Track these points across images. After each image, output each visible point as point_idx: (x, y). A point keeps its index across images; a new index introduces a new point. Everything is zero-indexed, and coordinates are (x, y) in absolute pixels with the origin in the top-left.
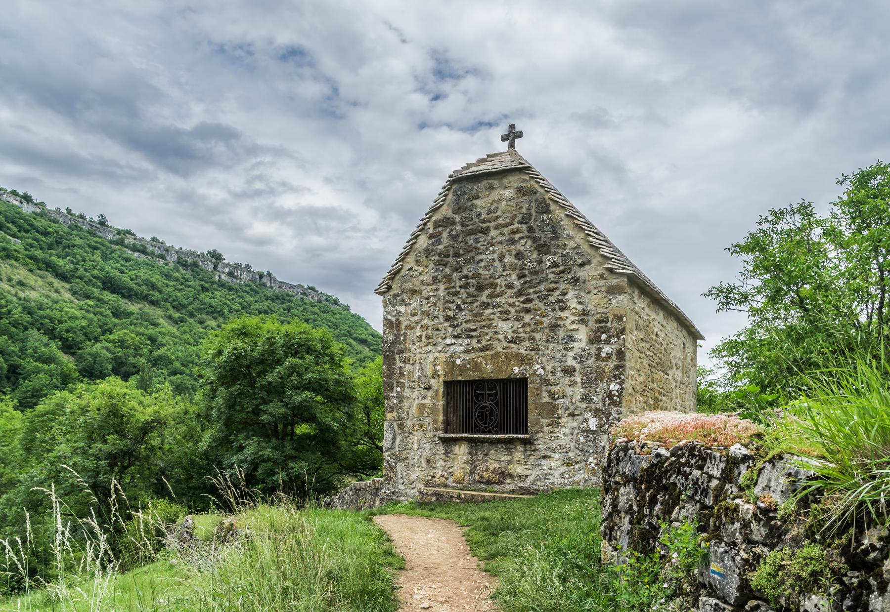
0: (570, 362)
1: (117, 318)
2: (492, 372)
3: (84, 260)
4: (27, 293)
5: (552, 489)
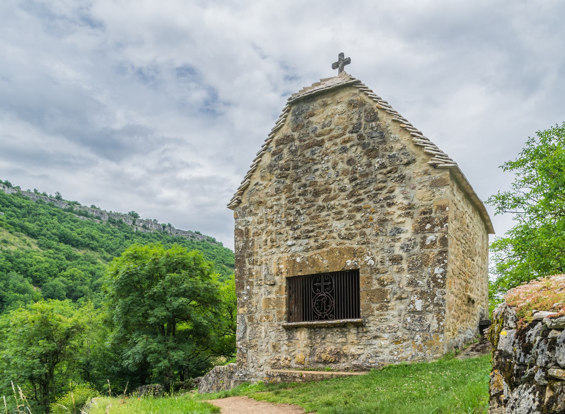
0: (398, 251)
1: (69, 260)
2: (328, 266)
3: (46, 223)
4: (9, 247)
5: (382, 365)
